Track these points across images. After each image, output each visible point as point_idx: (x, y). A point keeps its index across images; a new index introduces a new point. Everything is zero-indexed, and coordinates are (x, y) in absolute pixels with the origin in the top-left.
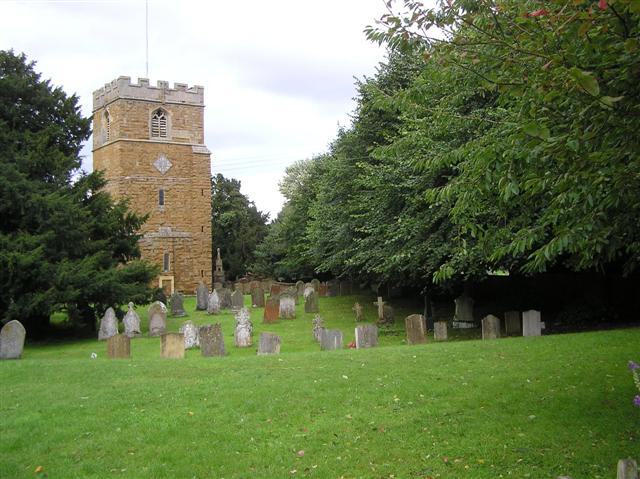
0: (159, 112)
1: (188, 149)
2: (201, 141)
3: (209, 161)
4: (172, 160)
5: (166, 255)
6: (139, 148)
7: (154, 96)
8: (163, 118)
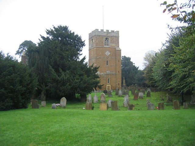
0: (107, 39)
1: (115, 49)
2: (119, 47)
3: (121, 52)
4: (110, 52)
5: (109, 79)
6: (101, 49)
7: (105, 34)
8: (108, 40)
